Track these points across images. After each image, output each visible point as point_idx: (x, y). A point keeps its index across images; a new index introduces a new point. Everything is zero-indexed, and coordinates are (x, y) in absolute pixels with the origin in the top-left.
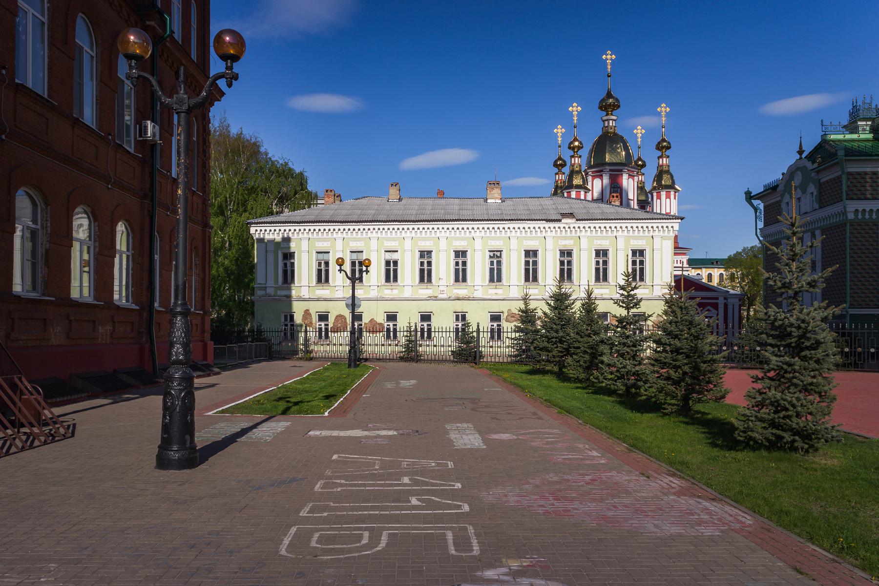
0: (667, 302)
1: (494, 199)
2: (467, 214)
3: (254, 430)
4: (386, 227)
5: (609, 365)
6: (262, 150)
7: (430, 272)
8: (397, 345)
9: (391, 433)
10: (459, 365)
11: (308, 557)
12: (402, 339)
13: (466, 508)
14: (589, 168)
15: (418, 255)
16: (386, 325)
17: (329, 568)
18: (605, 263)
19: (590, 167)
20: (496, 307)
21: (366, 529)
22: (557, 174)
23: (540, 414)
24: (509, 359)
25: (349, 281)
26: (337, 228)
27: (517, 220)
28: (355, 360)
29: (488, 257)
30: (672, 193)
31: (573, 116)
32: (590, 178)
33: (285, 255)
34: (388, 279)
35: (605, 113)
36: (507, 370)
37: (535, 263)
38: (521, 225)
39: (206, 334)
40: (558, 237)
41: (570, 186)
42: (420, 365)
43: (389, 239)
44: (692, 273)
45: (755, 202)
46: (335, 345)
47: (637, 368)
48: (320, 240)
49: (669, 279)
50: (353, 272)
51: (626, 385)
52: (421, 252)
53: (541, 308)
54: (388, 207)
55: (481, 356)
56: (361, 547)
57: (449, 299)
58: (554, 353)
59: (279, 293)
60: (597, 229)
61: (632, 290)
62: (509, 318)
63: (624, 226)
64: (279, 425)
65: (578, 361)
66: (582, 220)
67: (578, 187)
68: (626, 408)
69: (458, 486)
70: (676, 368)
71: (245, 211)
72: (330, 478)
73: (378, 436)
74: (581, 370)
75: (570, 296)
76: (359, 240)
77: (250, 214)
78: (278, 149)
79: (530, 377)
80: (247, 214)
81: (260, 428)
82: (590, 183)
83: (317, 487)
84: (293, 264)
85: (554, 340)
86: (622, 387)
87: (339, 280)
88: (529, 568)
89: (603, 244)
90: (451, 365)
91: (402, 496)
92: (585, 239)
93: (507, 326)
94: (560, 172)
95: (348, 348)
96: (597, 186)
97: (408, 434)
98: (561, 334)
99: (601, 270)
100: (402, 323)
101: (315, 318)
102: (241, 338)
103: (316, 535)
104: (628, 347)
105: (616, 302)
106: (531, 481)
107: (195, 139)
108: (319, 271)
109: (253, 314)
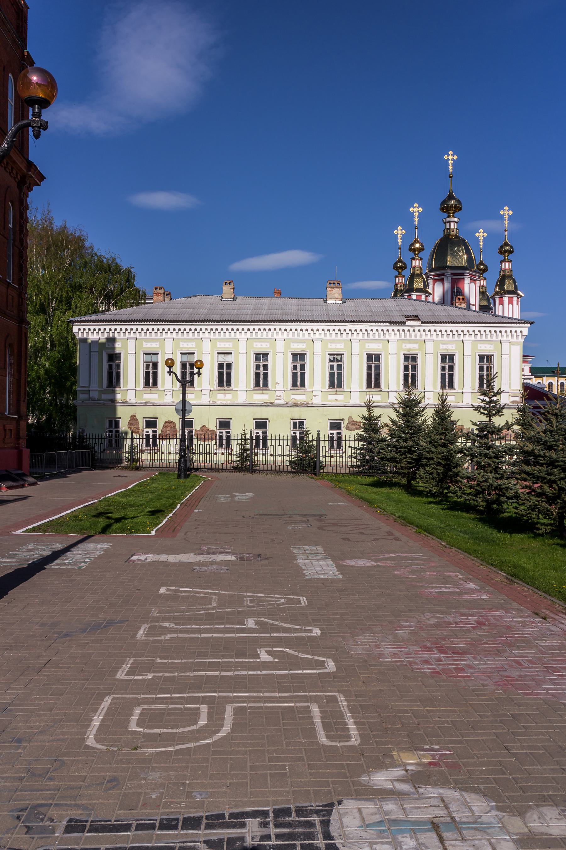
0: (519, 410)
1: (335, 298)
2: (305, 315)
3: (67, 554)
4: (219, 328)
5: (468, 478)
6: (87, 244)
7: (266, 375)
8: (230, 454)
9: (229, 558)
10: (297, 476)
11: (125, 750)
12: (236, 447)
13: (331, 666)
14: (430, 271)
15: (253, 357)
16: (218, 432)
17: (153, 769)
18: (451, 368)
19: (431, 270)
20: (336, 414)
21: (203, 700)
22: (397, 277)
23: (397, 534)
24: (352, 470)
25: (178, 384)
26: (166, 328)
27: (359, 322)
28: (185, 470)
29: (328, 361)
30: (515, 299)
31: (413, 217)
32: (431, 282)
33: (109, 355)
34: (220, 383)
35: (446, 215)
36: (350, 482)
37: (378, 368)
38: (364, 327)
39: (21, 441)
40: (403, 341)
41: (411, 289)
42: (255, 476)
43: (222, 340)
44: (534, 381)
46: (163, 453)
47: (500, 482)
48: (147, 340)
49: (517, 387)
50: (184, 374)
51: (487, 501)
52: (257, 354)
53: (387, 416)
54: (221, 306)
55: (322, 467)
56: (198, 731)
57: (286, 405)
58: (402, 464)
59: (103, 397)
60: (443, 332)
61: (495, 395)
62: (350, 426)
63: (471, 329)
64: (97, 548)
65: (431, 474)
66: (428, 323)
67: (419, 290)
68: (490, 527)
69: (317, 631)
70: (551, 483)
71: (70, 309)
72: (156, 620)
73: (214, 562)
74: (434, 483)
75: (420, 402)
76: (191, 340)
77: (74, 312)
78: (103, 244)
79: (376, 490)
80: (69, 313)
81: (75, 551)
82: (431, 287)
83: (140, 635)
84: (118, 366)
85: (403, 450)
86: (482, 503)
87: (168, 383)
88: (433, 768)
89: (449, 349)
90: (289, 475)
91: (247, 648)
92: (430, 342)
93: (349, 435)
94: (399, 275)
95: (177, 457)
96: (438, 291)
97: (249, 559)
98: (410, 443)
99: (447, 376)
100: (236, 431)
101: (142, 424)
102: (62, 444)
103: (138, 711)
104: (490, 458)
105: (477, 409)
106: (405, 624)
107: (10, 226)
108: (147, 374)
109: (75, 419)
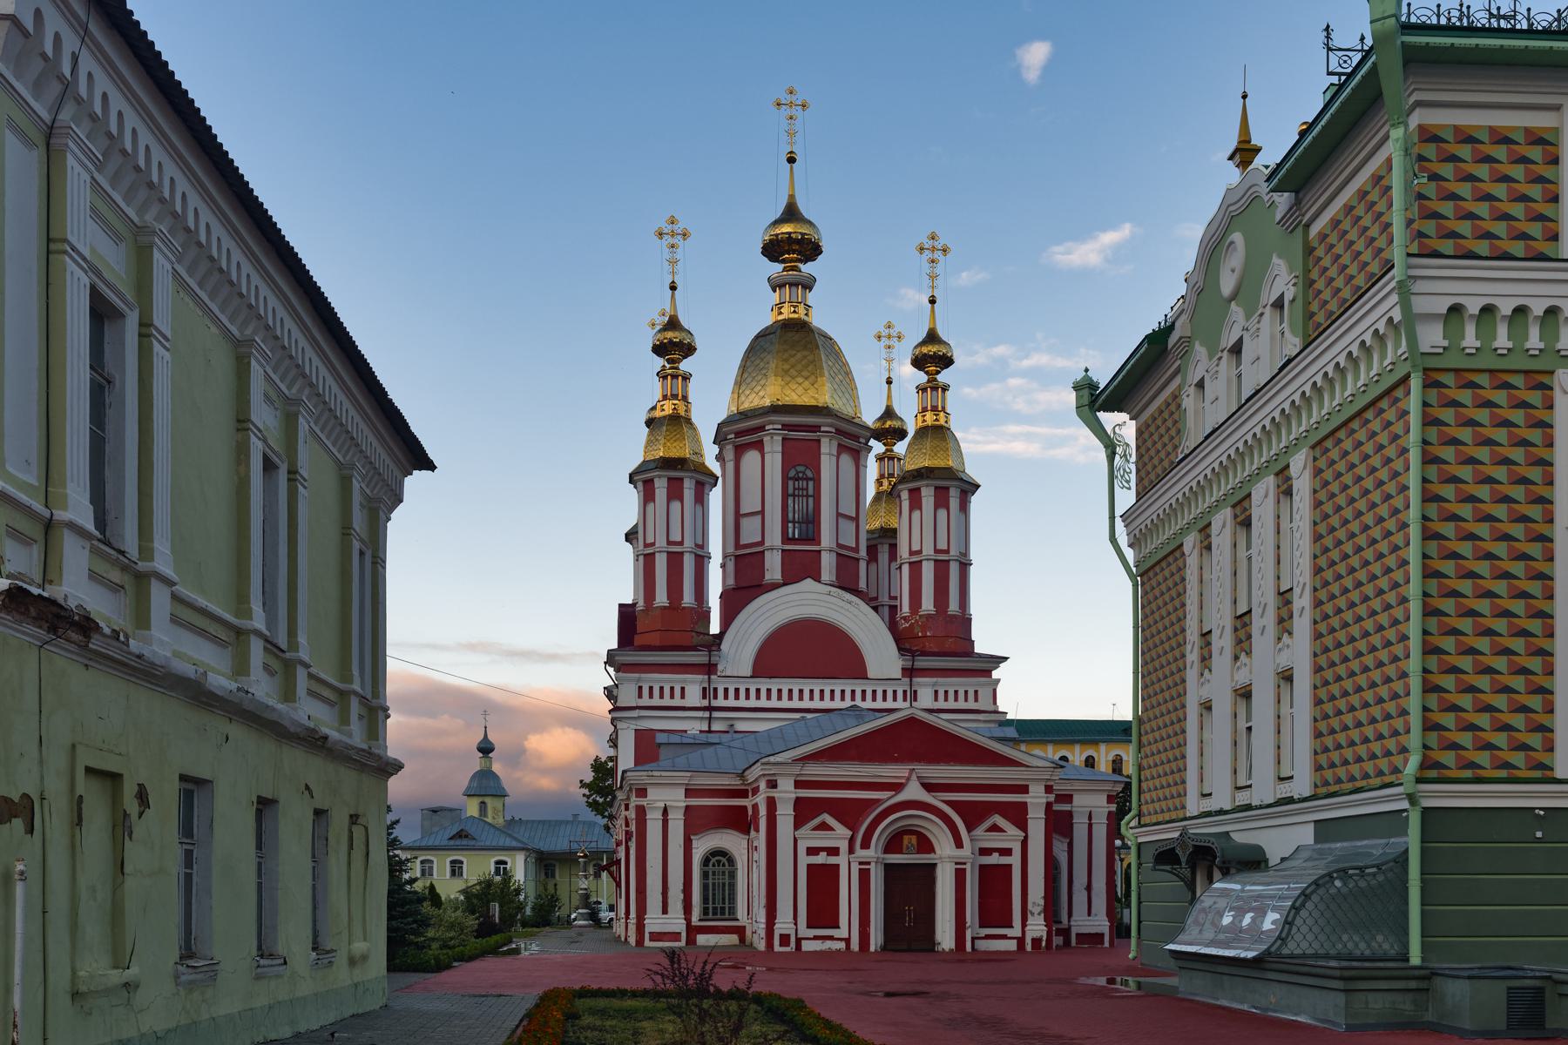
45: (1109, 419)
